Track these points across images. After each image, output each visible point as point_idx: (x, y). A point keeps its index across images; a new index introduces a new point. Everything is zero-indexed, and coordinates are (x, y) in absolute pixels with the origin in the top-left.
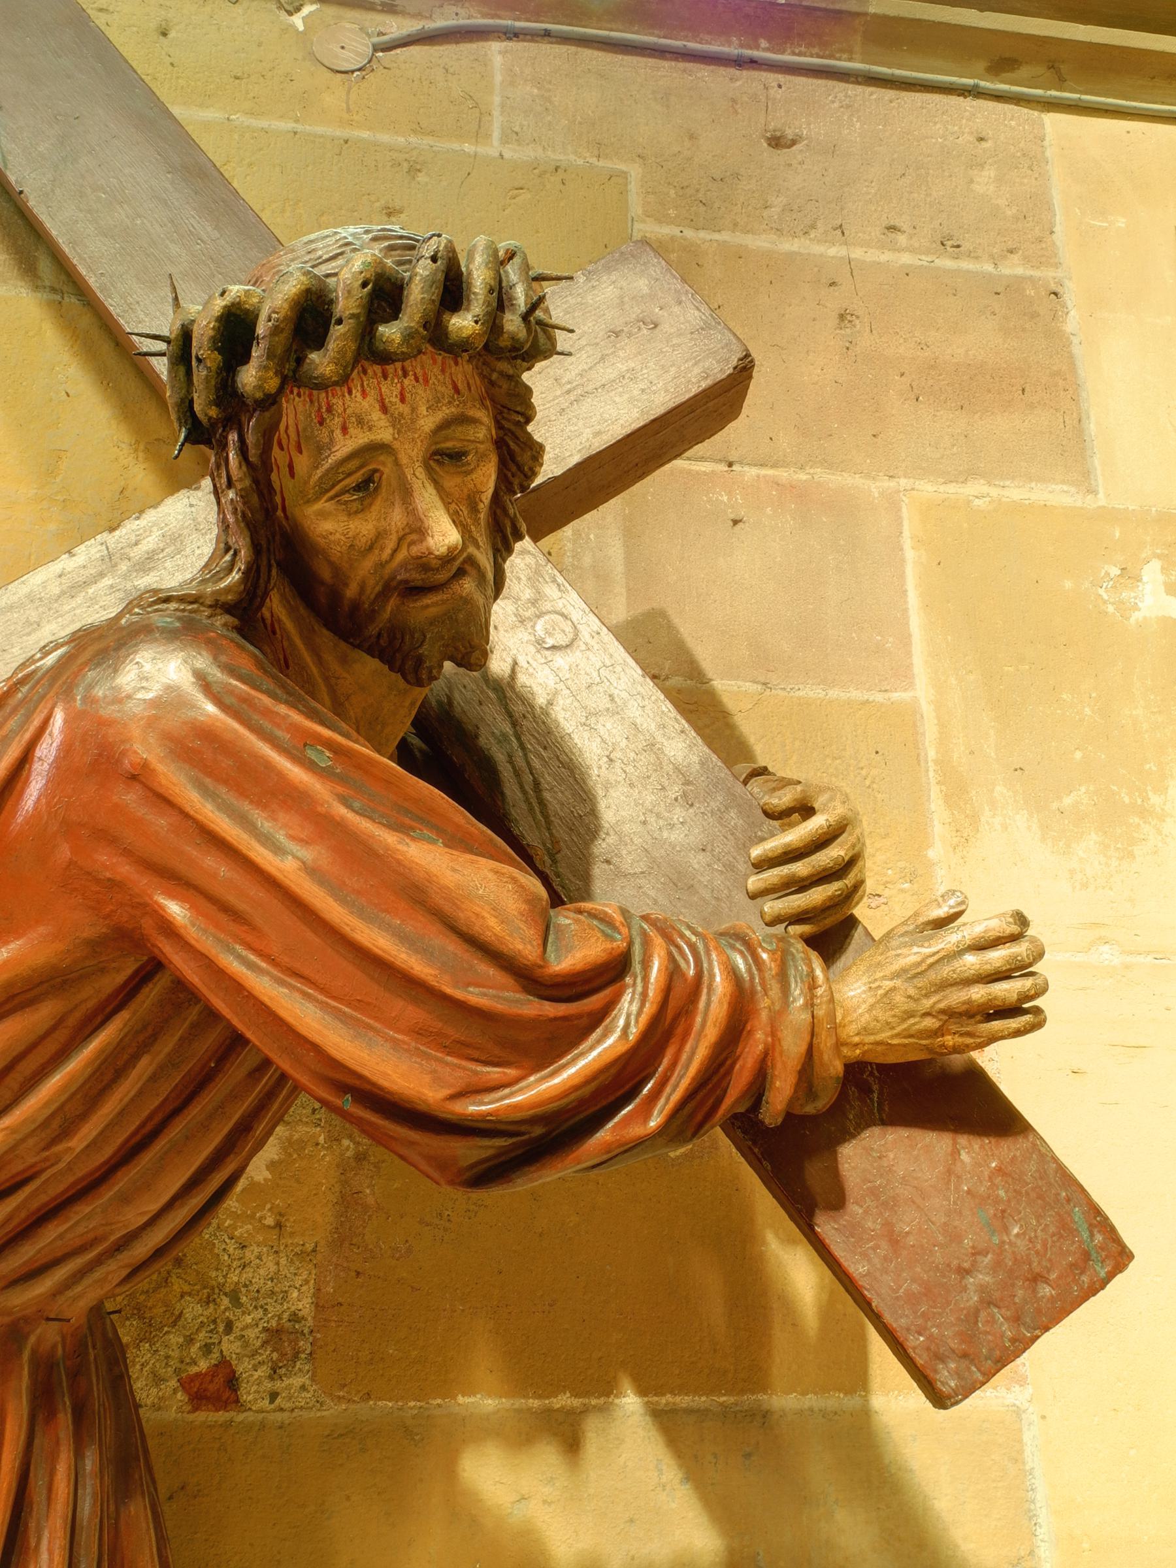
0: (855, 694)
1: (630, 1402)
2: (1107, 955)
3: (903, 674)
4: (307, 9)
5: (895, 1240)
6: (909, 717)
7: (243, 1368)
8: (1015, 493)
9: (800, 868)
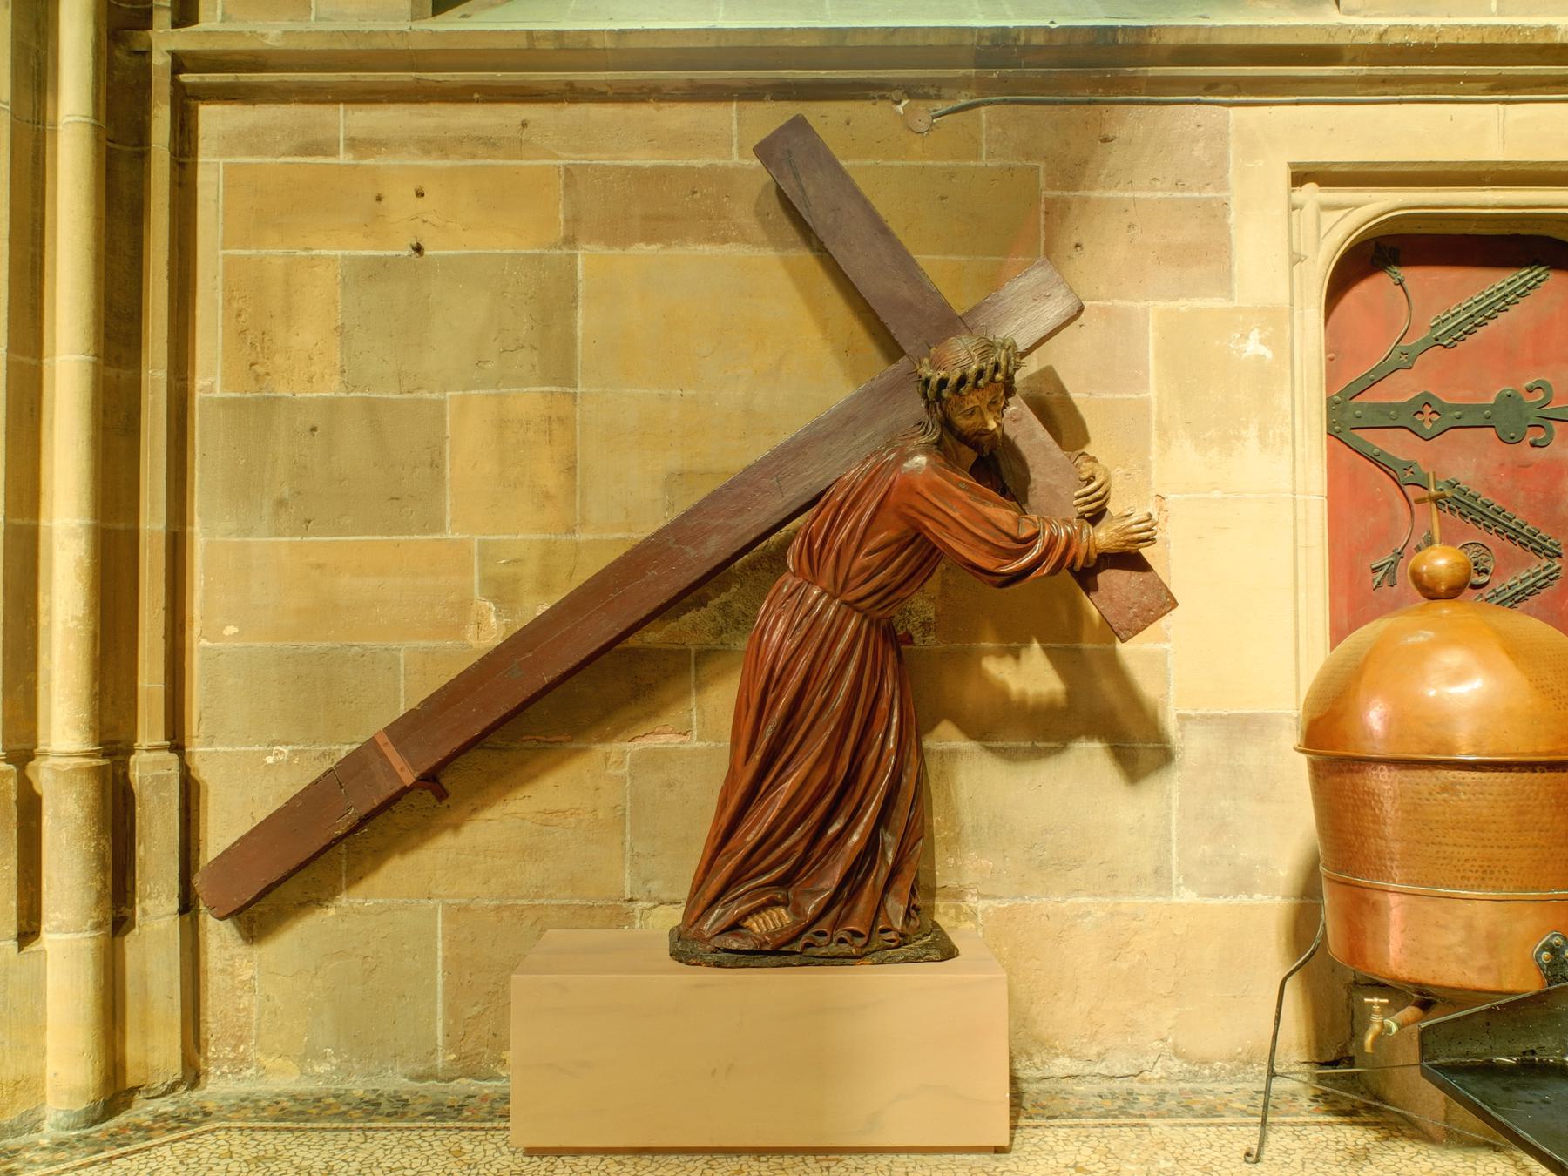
0: (1125, 396)
1: (1036, 645)
2: (1217, 494)
3: (1145, 386)
4: (904, 103)
5: (1111, 599)
6: (1144, 405)
7: (914, 633)
8: (1198, 303)
9: (1089, 498)
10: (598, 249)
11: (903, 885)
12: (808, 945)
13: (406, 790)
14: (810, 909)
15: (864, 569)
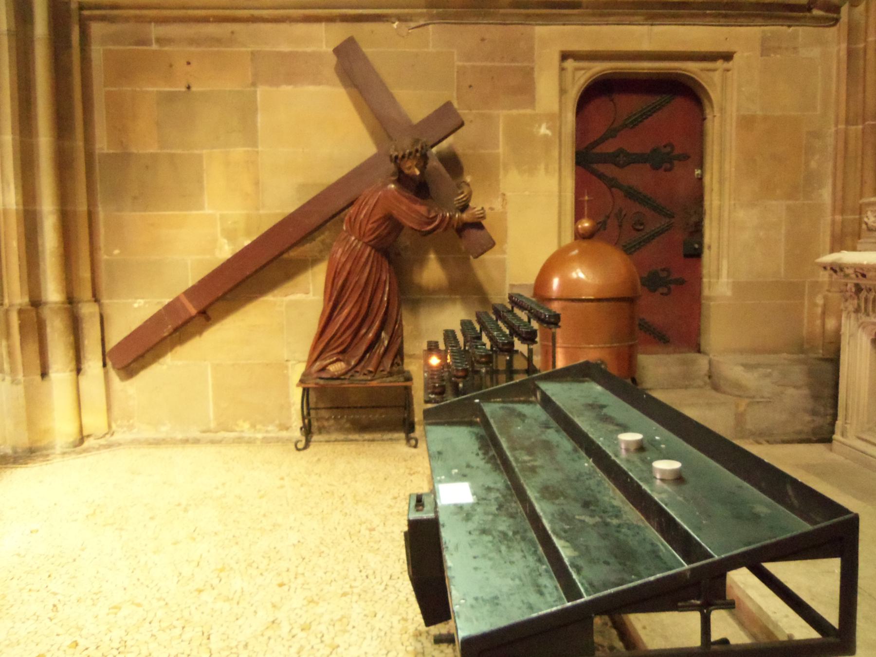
3: (498, 147)
4: (397, 23)
8: (522, 111)
10: (266, 88)
11: (391, 354)
12: (352, 376)
13: (192, 318)
14: (353, 363)
15: (370, 230)
